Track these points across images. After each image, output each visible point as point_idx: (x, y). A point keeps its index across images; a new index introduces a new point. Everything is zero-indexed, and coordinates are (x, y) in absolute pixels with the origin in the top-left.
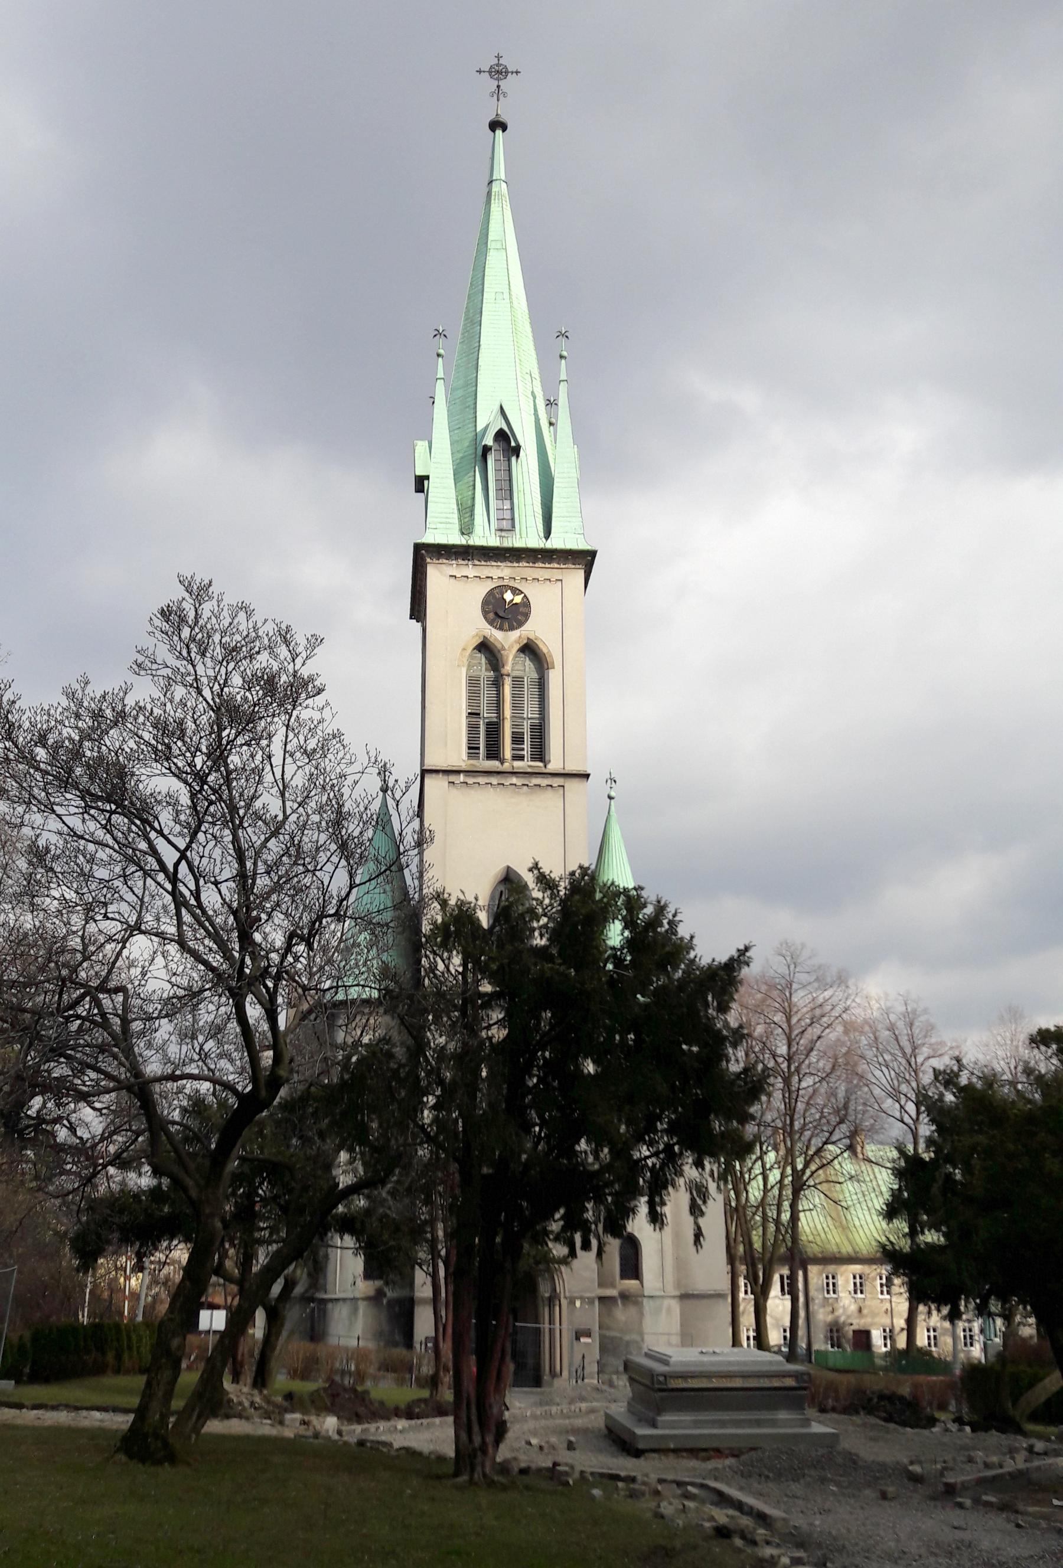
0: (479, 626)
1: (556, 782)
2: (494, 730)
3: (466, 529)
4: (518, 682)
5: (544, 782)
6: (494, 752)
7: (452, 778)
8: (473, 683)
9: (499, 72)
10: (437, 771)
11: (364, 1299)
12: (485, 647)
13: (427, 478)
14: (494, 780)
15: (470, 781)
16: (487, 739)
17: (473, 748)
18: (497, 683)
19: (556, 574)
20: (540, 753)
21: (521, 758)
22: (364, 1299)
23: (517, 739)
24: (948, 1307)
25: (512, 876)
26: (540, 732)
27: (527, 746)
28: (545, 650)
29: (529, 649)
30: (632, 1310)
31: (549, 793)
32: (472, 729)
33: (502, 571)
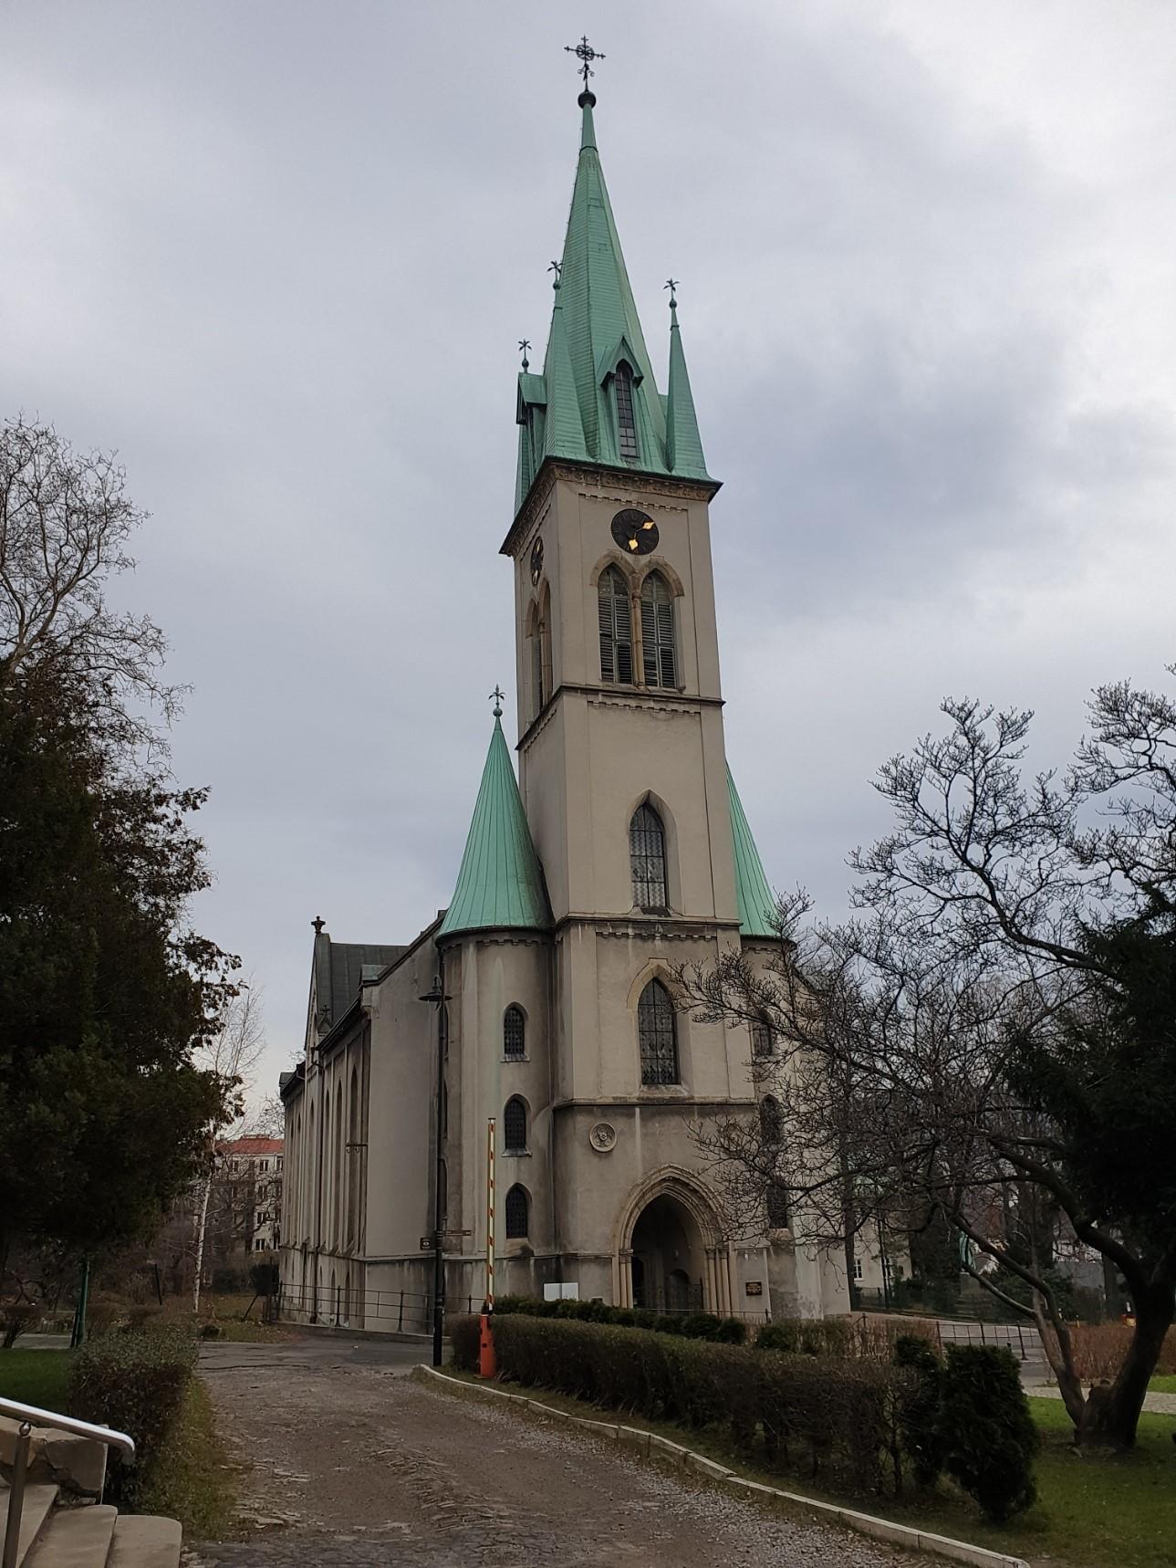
0: (606, 545)
1: (693, 708)
2: (625, 653)
3: (592, 449)
4: (646, 607)
5: (681, 708)
6: (626, 676)
7: (591, 698)
8: (603, 605)
9: (585, 53)
10: (575, 689)
11: (510, 1259)
12: (612, 568)
13: (543, 408)
14: (633, 703)
15: (609, 701)
16: (618, 661)
17: (606, 670)
18: (625, 609)
19: (682, 504)
20: (670, 677)
21: (654, 683)
22: (510, 1259)
23: (649, 665)
24: (1172, 900)
25: (653, 802)
26: (669, 658)
27: (659, 671)
28: (522, 886)
29: (656, 574)
30: (785, 1258)
31: (686, 719)
32: (605, 651)
33: (630, 497)
